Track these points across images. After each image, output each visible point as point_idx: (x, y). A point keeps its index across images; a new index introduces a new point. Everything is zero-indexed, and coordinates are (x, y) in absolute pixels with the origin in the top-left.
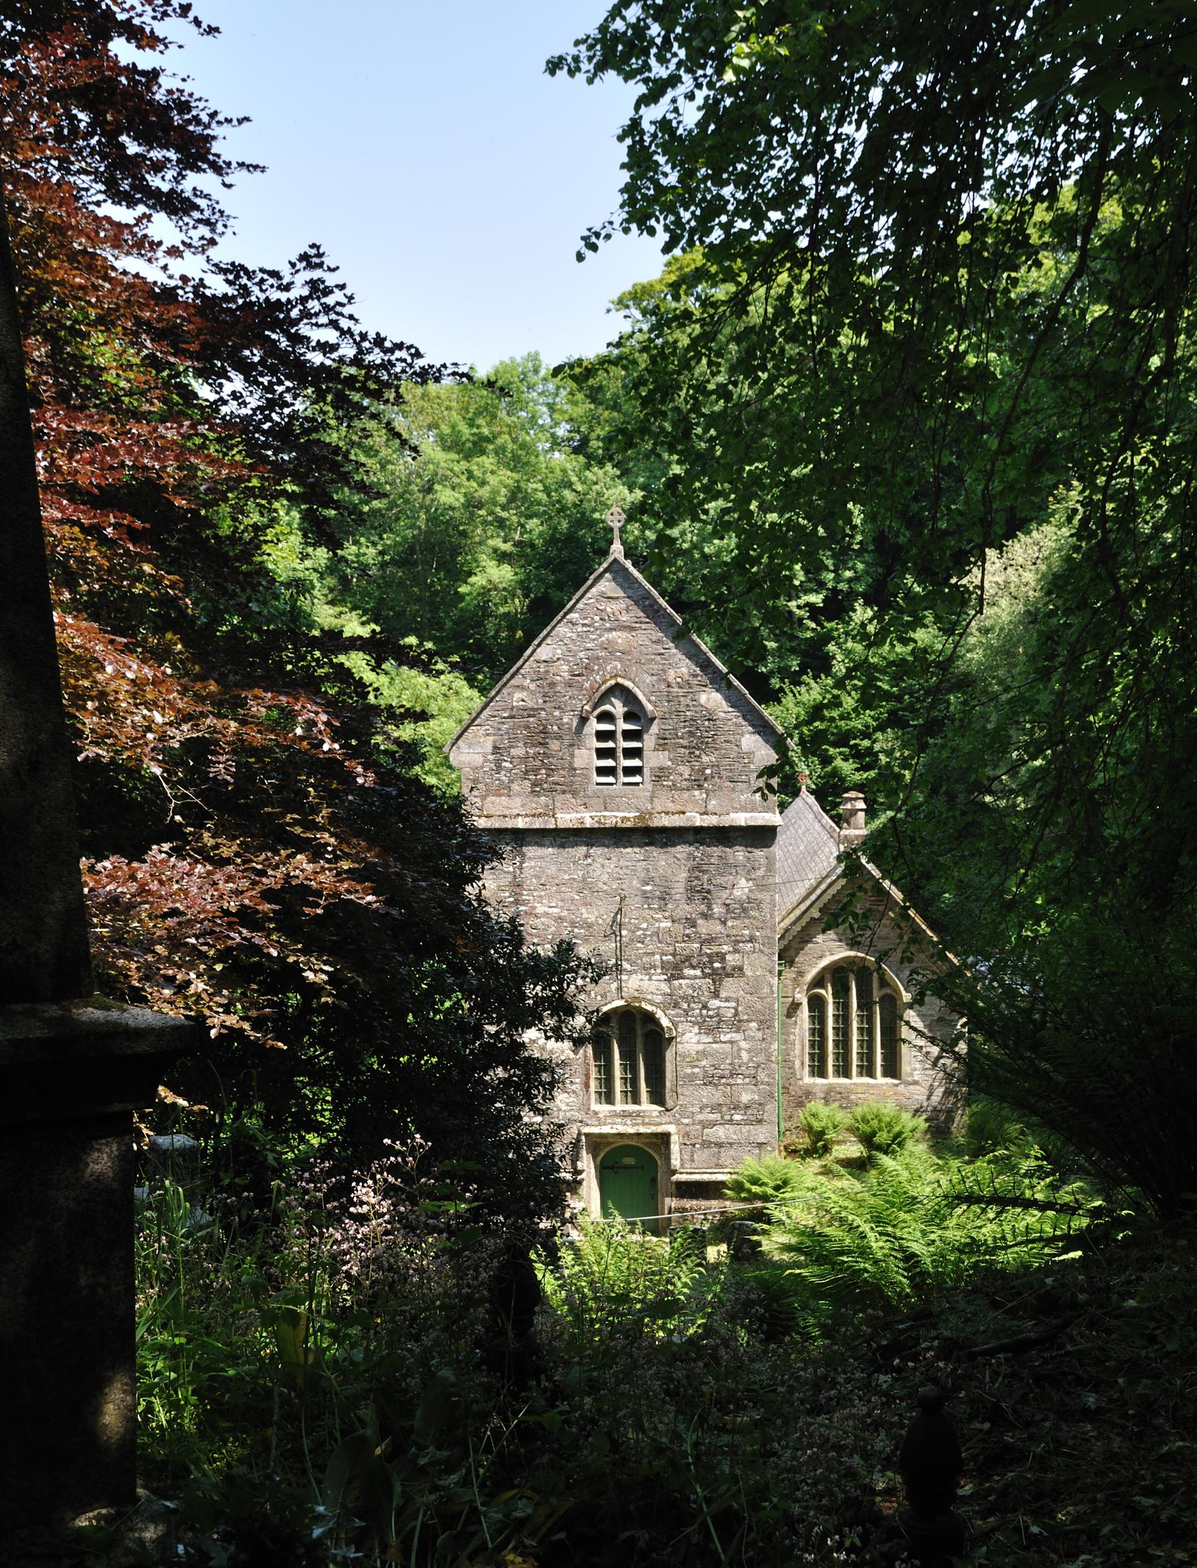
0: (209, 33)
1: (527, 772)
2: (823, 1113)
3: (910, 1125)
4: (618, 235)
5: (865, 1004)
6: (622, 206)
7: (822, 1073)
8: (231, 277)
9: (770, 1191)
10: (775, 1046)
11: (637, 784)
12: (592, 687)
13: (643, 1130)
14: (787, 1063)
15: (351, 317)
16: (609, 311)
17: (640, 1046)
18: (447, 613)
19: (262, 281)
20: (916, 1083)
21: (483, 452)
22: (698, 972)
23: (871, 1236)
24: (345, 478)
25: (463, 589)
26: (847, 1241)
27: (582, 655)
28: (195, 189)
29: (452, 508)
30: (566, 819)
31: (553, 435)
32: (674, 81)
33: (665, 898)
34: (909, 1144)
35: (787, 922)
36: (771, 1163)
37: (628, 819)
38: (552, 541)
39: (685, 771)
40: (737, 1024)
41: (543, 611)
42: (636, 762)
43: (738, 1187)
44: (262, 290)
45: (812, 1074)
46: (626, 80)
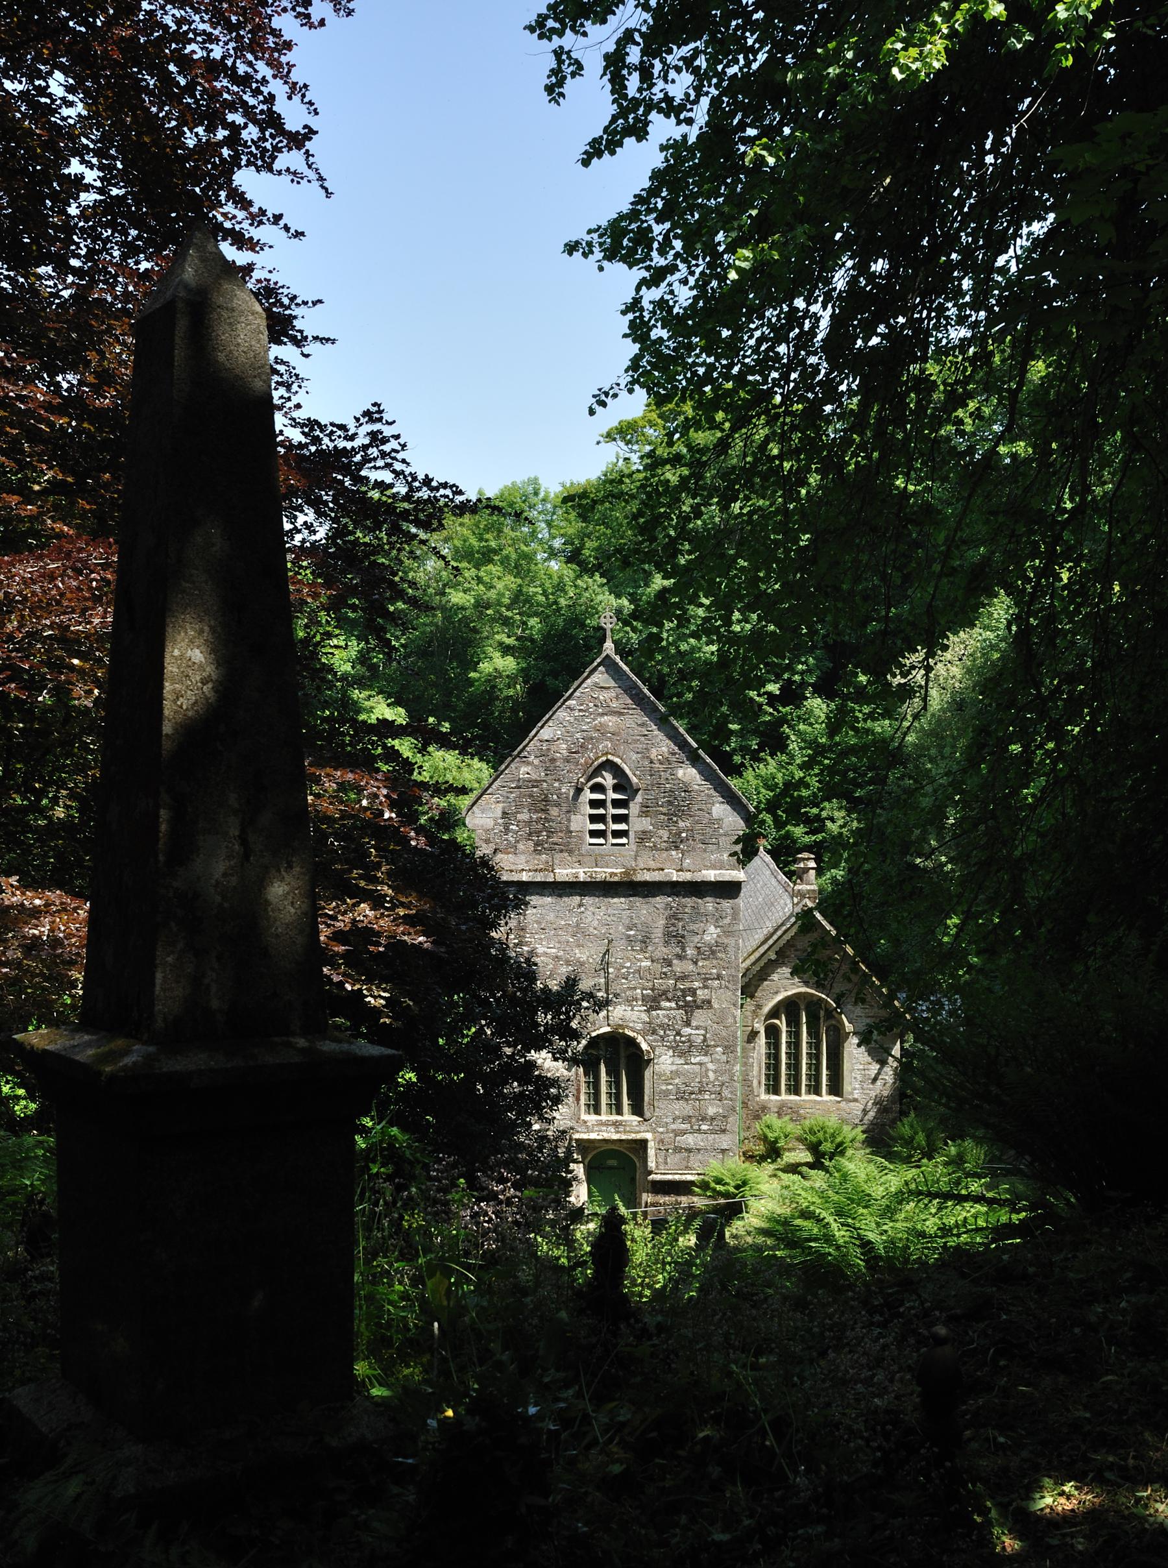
0: (295, 237)
1: (530, 834)
2: (777, 1125)
3: (850, 1136)
4: (624, 394)
5: (814, 1033)
6: (626, 371)
7: (776, 1092)
8: (306, 430)
9: (732, 1190)
10: (738, 1067)
11: (624, 845)
12: (586, 763)
13: (624, 1137)
14: (747, 1082)
15: (404, 461)
16: (598, 443)
17: (623, 1062)
18: (458, 698)
19: (332, 432)
20: (856, 1100)
21: (491, 561)
22: (673, 1005)
23: (834, 1226)
24: (400, 595)
25: (472, 675)
26: (815, 1231)
27: (578, 735)
28: (276, 358)
29: (463, 608)
30: (564, 873)
31: (550, 547)
32: (672, 269)
33: (645, 941)
34: (849, 1152)
35: (748, 962)
36: (733, 1166)
37: (616, 874)
38: (547, 637)
39: (665, 834)
40: (705, 1049)
41: (542, 697)
42: (622, 827)
43: (705, 1186)
44: (331, 440)
45: (768, 1091)
46: (630, 268)
